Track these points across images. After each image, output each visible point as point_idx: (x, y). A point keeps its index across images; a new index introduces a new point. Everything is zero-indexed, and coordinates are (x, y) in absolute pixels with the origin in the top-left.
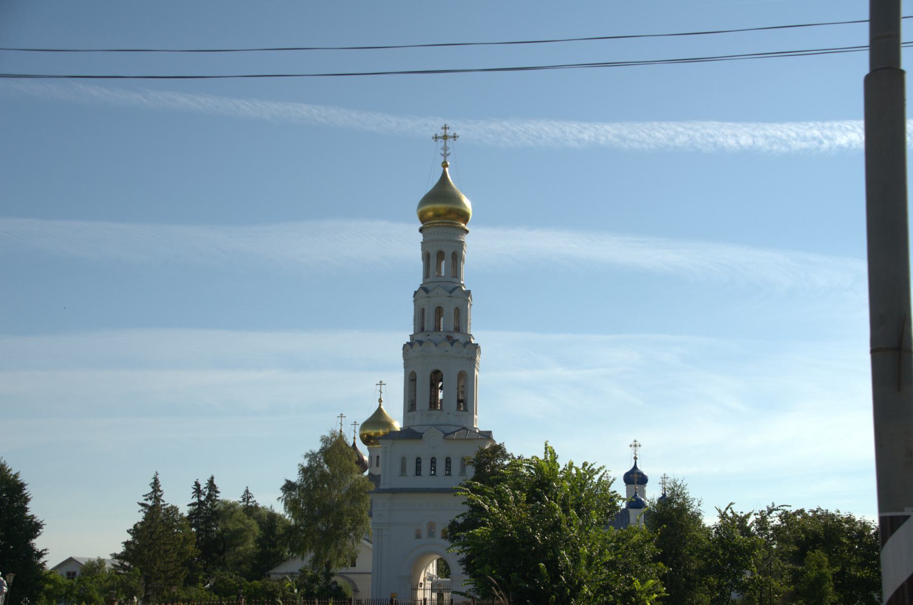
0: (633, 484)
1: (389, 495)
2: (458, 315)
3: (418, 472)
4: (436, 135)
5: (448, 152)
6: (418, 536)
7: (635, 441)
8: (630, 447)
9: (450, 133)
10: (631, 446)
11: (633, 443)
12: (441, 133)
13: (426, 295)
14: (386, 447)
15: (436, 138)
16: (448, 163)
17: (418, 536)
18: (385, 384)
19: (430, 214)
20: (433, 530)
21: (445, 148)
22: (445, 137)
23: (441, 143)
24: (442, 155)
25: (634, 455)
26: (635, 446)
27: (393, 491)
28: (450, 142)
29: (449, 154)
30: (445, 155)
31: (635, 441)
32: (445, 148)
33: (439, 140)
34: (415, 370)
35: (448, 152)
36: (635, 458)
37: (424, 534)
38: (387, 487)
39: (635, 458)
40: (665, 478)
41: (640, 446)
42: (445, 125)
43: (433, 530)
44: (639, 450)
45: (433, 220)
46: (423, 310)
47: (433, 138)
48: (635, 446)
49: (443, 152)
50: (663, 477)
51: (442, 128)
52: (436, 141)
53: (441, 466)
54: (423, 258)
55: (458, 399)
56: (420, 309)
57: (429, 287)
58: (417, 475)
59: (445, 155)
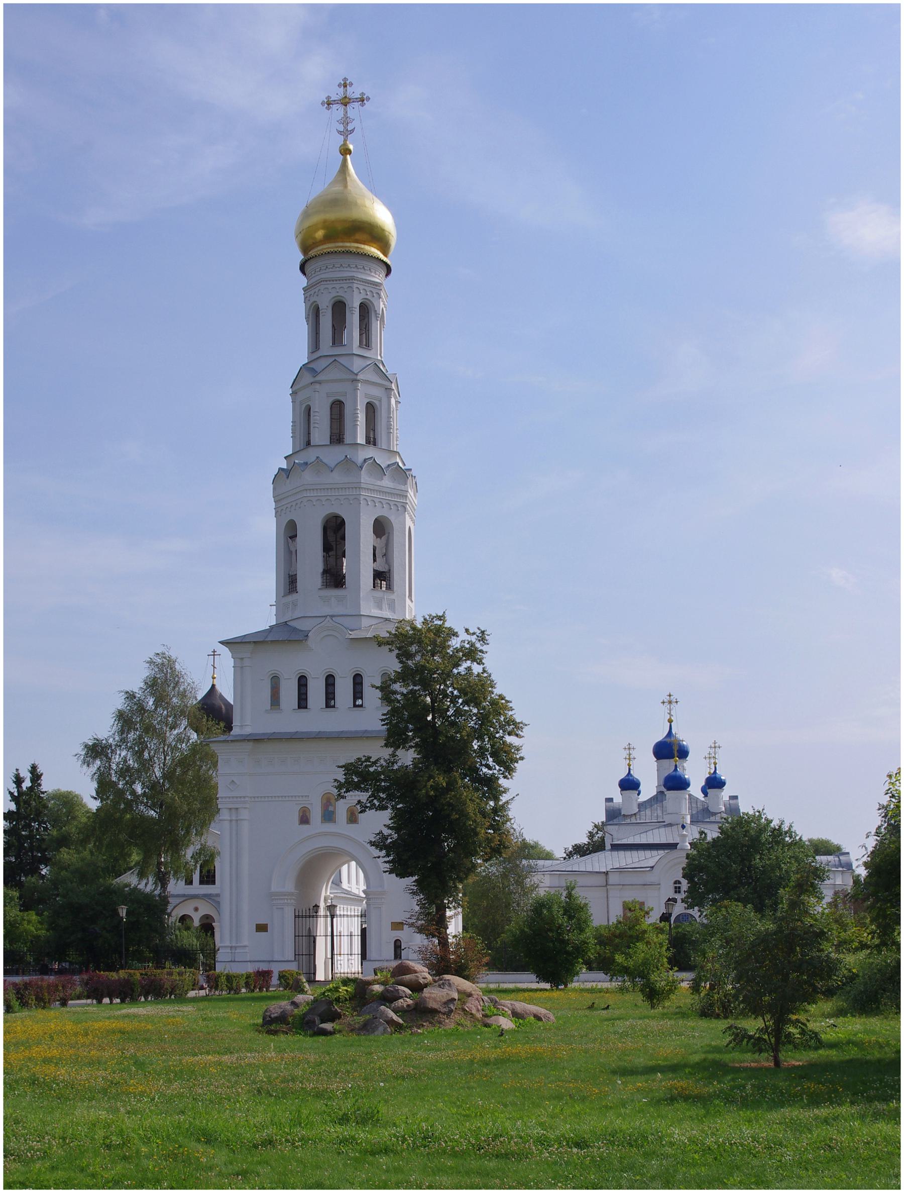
0: (672, 757)
1: (250, 745)
2: (347, 738)
3: (303, 702)
4: (329, 97)
5: (350, 128)
6: (304, 819)
7: (670, 696)
8: (662, 704)
9: (354, 92)
10: (663, 702)
11: (667, 699)
12: (337, 94)
13: (312, 380)
14: (242, 659)
15: (329, 103)
16: (351, 147)
17: (304, 819)
18: (220, 655)
19: (320, 234)
20: (331, 809)
21: (346, 121)
22: (345, 102)
23: (338, 111)
24: (340, 132)
25: (668, 717)
26: (670, 702)
27: (257, 740)
28: (354, 110)
29: (353, 130)
30: (346, 133)
31: (670, 696)
32: (346, 121)
33: (334, 107)
34: (311, 405)
35: (350, 128)
36: (670, 721)
37: (316, 814)
38: (248, 730)
39: (670, 721)
40: (715, 747)
41: (677, 702)
42: (345, 79)
43: (331, 809)
44: (676, 710)
45: (325, 243)
46: (308, 410)
47: (323, 104)
48: (670, 702)
49: (341, 128)
50: (713, 746)
51: (339, 85)
52: (328, 109)
53: (344, 689)
54: (307, 318)
55: (362, 700)
56: (304, 406)
57: (319, 365)
58: (300, 707)
59: (346, 133)
